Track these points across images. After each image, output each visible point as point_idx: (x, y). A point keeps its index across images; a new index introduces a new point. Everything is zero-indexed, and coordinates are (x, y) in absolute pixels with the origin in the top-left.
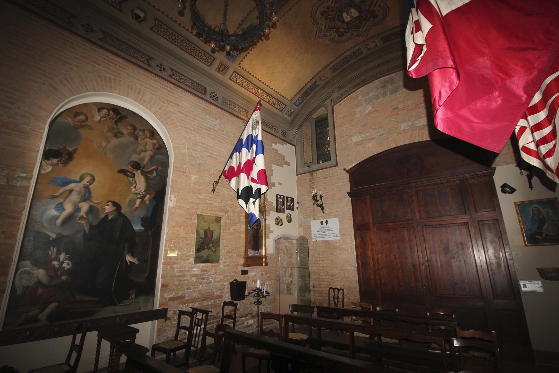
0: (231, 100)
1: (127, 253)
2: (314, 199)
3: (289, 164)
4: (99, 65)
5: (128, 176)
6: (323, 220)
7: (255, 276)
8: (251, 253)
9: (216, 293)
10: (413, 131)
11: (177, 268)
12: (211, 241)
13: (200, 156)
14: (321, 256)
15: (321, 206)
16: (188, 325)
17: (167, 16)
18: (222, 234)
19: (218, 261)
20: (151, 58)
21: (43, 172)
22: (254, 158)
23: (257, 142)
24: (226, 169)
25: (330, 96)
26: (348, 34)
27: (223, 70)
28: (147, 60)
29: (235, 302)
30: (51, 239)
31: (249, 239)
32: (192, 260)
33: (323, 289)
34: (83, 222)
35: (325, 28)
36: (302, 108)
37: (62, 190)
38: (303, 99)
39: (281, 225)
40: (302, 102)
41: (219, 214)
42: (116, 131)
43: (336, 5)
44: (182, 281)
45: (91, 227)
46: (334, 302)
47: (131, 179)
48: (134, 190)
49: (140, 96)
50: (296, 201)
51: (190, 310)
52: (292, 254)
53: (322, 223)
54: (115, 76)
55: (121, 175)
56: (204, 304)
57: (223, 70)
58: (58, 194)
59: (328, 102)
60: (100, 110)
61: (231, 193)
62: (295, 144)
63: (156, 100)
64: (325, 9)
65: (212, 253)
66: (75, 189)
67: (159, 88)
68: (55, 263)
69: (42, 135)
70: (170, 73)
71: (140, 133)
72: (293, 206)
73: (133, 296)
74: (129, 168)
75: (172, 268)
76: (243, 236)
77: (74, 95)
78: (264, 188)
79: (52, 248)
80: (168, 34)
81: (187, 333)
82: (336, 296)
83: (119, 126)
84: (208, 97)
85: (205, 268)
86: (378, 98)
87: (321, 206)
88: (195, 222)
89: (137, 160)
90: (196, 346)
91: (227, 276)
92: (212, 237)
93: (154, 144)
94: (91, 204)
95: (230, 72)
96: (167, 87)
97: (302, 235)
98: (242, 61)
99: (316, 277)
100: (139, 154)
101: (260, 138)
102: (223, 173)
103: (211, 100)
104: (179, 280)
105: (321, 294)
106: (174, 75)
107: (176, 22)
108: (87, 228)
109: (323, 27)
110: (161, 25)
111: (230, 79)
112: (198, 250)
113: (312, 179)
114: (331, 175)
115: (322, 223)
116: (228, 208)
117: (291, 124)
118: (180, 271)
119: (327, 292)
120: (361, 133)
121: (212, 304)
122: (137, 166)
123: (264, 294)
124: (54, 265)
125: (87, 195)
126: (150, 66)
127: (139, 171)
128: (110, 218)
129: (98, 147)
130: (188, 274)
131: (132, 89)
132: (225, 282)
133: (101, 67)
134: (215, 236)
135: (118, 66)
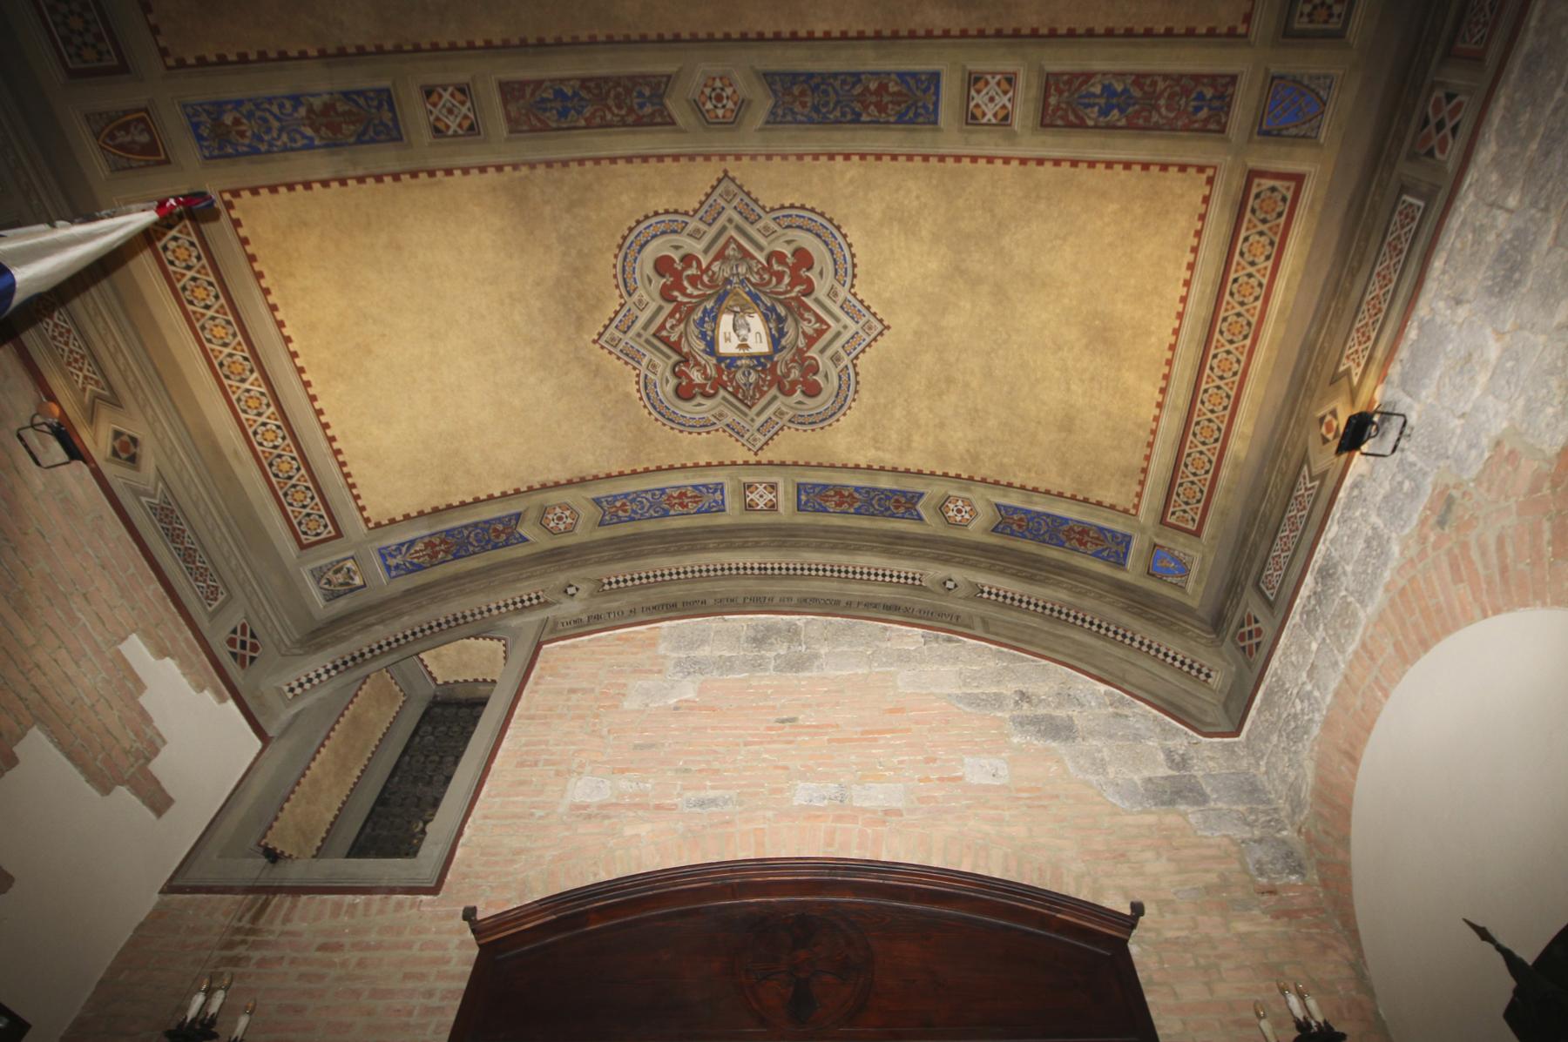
10: (839, 818)
25: (547, 604)
26: (709, 403)
35: (645, 327)
36: (408, 594)
38: (434, 560)
40: (419, 568)
43: (715, 267)
62: (272, 731)
64: (676, 256)
86: (731, 669)
95: (118, 97)
109: (644, 317)
114: (373, 937)
120: (622, 771)
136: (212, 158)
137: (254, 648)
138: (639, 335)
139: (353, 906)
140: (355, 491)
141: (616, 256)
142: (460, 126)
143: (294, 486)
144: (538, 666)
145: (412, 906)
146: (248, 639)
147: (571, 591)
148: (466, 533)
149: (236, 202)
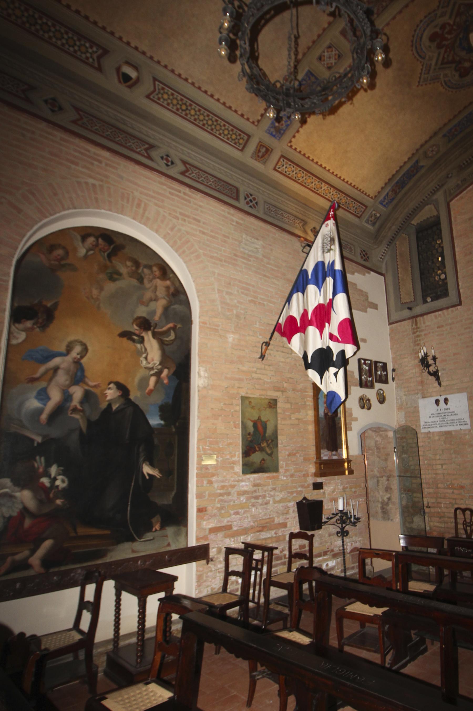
0: (279, 205)
1: (144, 461)
2: (422, 364)
3: (375, 307)
4: (76, 164)
5: (134, 341)
6: (438, 398)
7: (333, 492)
8: (326, 455)
9: (277, 521)
11: (217, 481)
12: (264, 438)
13: (239, 302)
14: (438, 457)
15: (435, 374)
16: (240, 568)
17: (173, 71)
18: (279, 427)
19: (276, 470)
20: (152, 147)
21: (14, 342)
22: (331, 301)
23: (333, 273)
24: (282, 321)
25: (443, 185)
27: (263, 156)
28: (146, 150)
29: (309, 533)
30: (35, 444)
31: (321, 433)
32: (238, 468)
33: (444, 510)
34: (77, 416)
35: (436, 64)
37: (42, 369)
39: (369, 408)
40: (393, 199)
41: (273, 394)
42: (110, 270)
44: (225, 502)
45: (90, 424)
46: (466, 531)
47: (139, 346)
48: (144, 362)
49: (141, 211)
50: (390, 367)
51: (242, 546)
52: (388, 455)
53: (437, 402)
54: (102, 181)
55: (125, 340)
56: (261, 537)
57: (263, 156)
58: (38, 375)
59: (440, 196)
60: (84, 239)
61: (288, 360)
62: (384, 272)
63: (164, 216)
64: (438, 30)
65: (266, 457)
66: (62, 366)
67: (168, 194)
68: (45, 481)
69: (8, 285)
70: (181, 167)
71: (146, 271)
72: (386, 375)
73: (157, 527)
74: (135, 328)
75: (210, 482)
76: (311, 428)
77: (46, 217)
78: (349, 349)
79: (38, 458)
80: (175, 102)
81: (240, 580)
82: (468, 521)
83: (114, 262)
84: (242, 204)
85: (258, 482)
87: (435, 374)
88: (239, 408)
89: (144, 315)
90: (256, 600)
91: (292, 493)
92: (265, 432)
93: (168, 288)
94: (87, 388)
95: (275, 157)
96: (180, 192)
97: (403, 422)
98: (294, 137)
99: (431, 490)
100: (147, 306)
101: (338, 266)
102: (278, 328)
103: (247, 208)
104: (222, 501)
105: (440, 518)
106: (187, 171)
107: (186, 80)
108: (83, 425)
109: (434, 62)
110: (163, 89)
111: (275, 169)
112: (247, 453)
113: (416, 329)
115: (437, 402)
116: (285, 385)
117: (376, 237)
118: (223, 487)
119: (452, 515)
121: (271, 538)
122: (145, 324)
123: (352, 519)
124: (43, 484)
125: (79, 374)
126: (149, 158)
127: (150, 333)
128: (114, 407)
129: (88, 298)
130: (233, 491)
131: (128, 202)
132: (289, 501)
133: (80, 169)
134: (269, 431)
135: (103, 165)
136: (280, 138)
137: (366, 254)
138: (435, 69)
139: (440, 315)
140: (364, 193)
141: (412, 51)
142: (335, 59)
143: (349, 204)
144: (452, 213)
145: (456, 310)
146: (364, 253)
147: (449, 176)
148: (402, 179)
149: (292, 144)
